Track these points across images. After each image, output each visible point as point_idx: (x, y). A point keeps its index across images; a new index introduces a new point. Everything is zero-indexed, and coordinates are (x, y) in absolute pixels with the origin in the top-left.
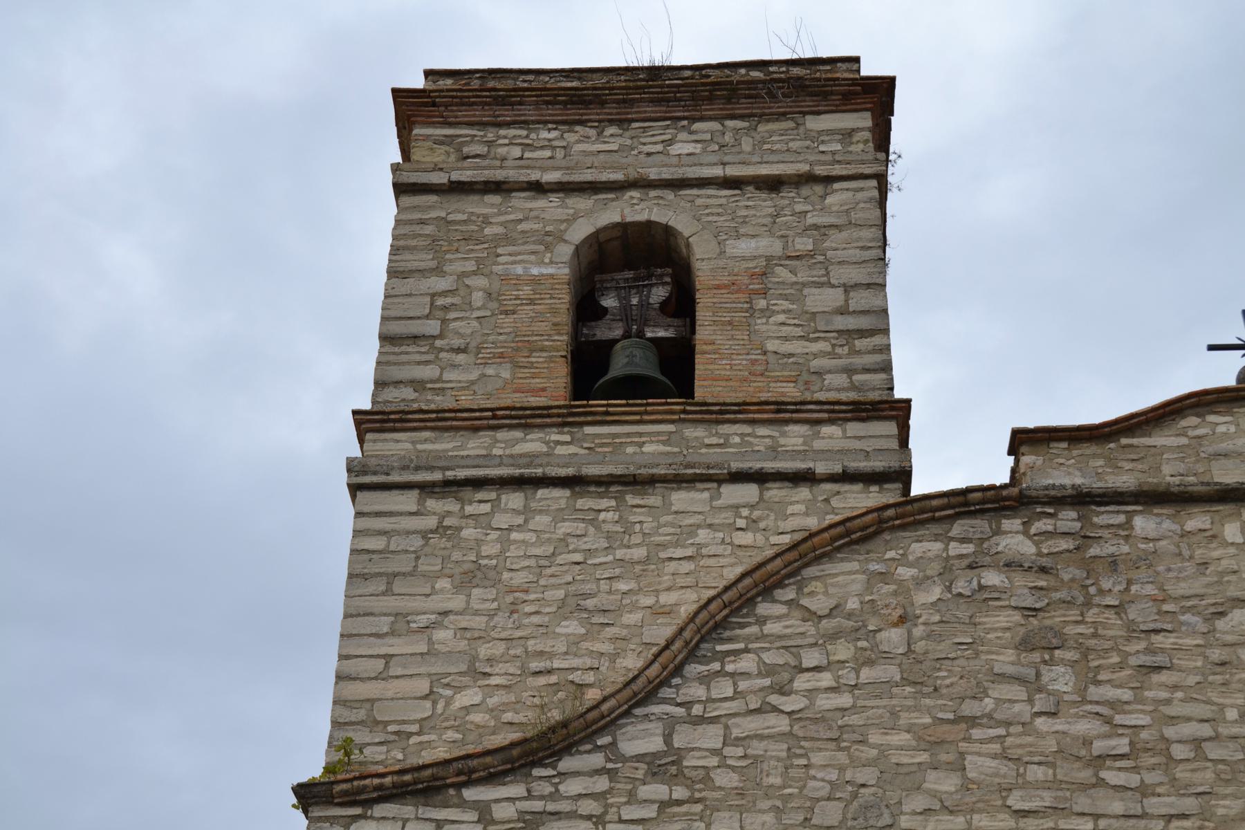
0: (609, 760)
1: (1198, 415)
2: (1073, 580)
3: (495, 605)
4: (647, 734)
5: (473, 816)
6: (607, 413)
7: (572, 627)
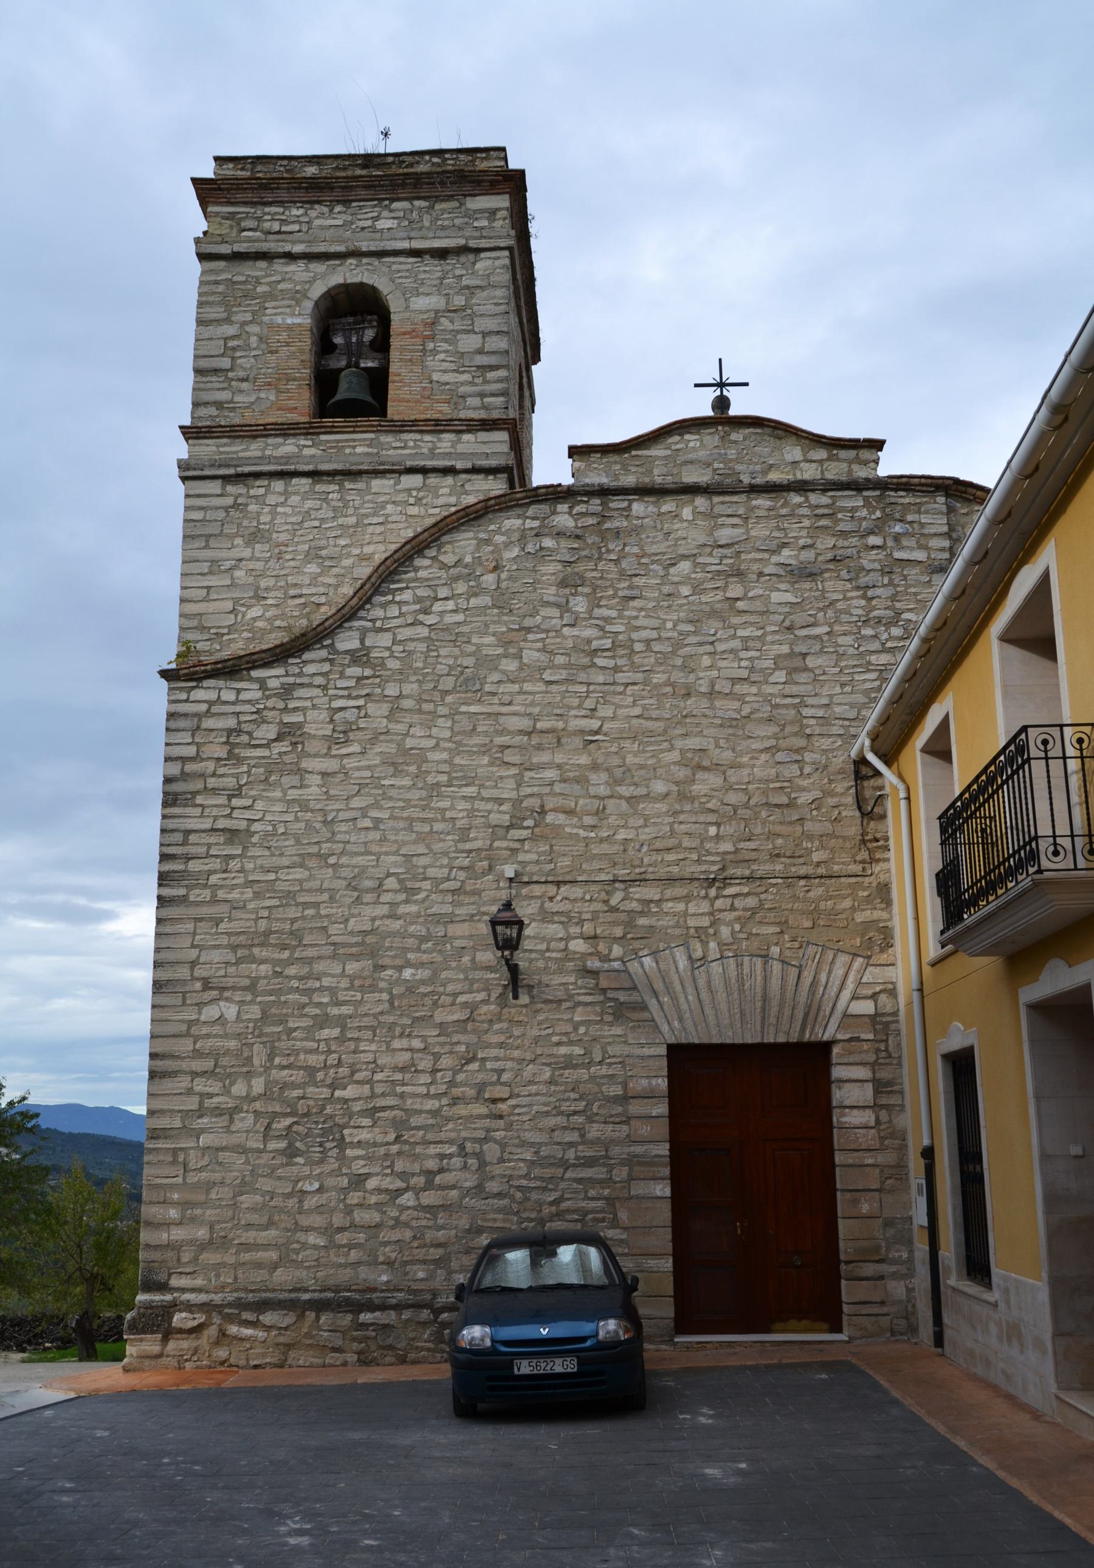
0: (330, 654)
1: (680, 435)
2: (593, 543)
3: (269, 555)
4: (351, 638)
5: (256, 686)
6: (334, 427)
7: (312, 568)
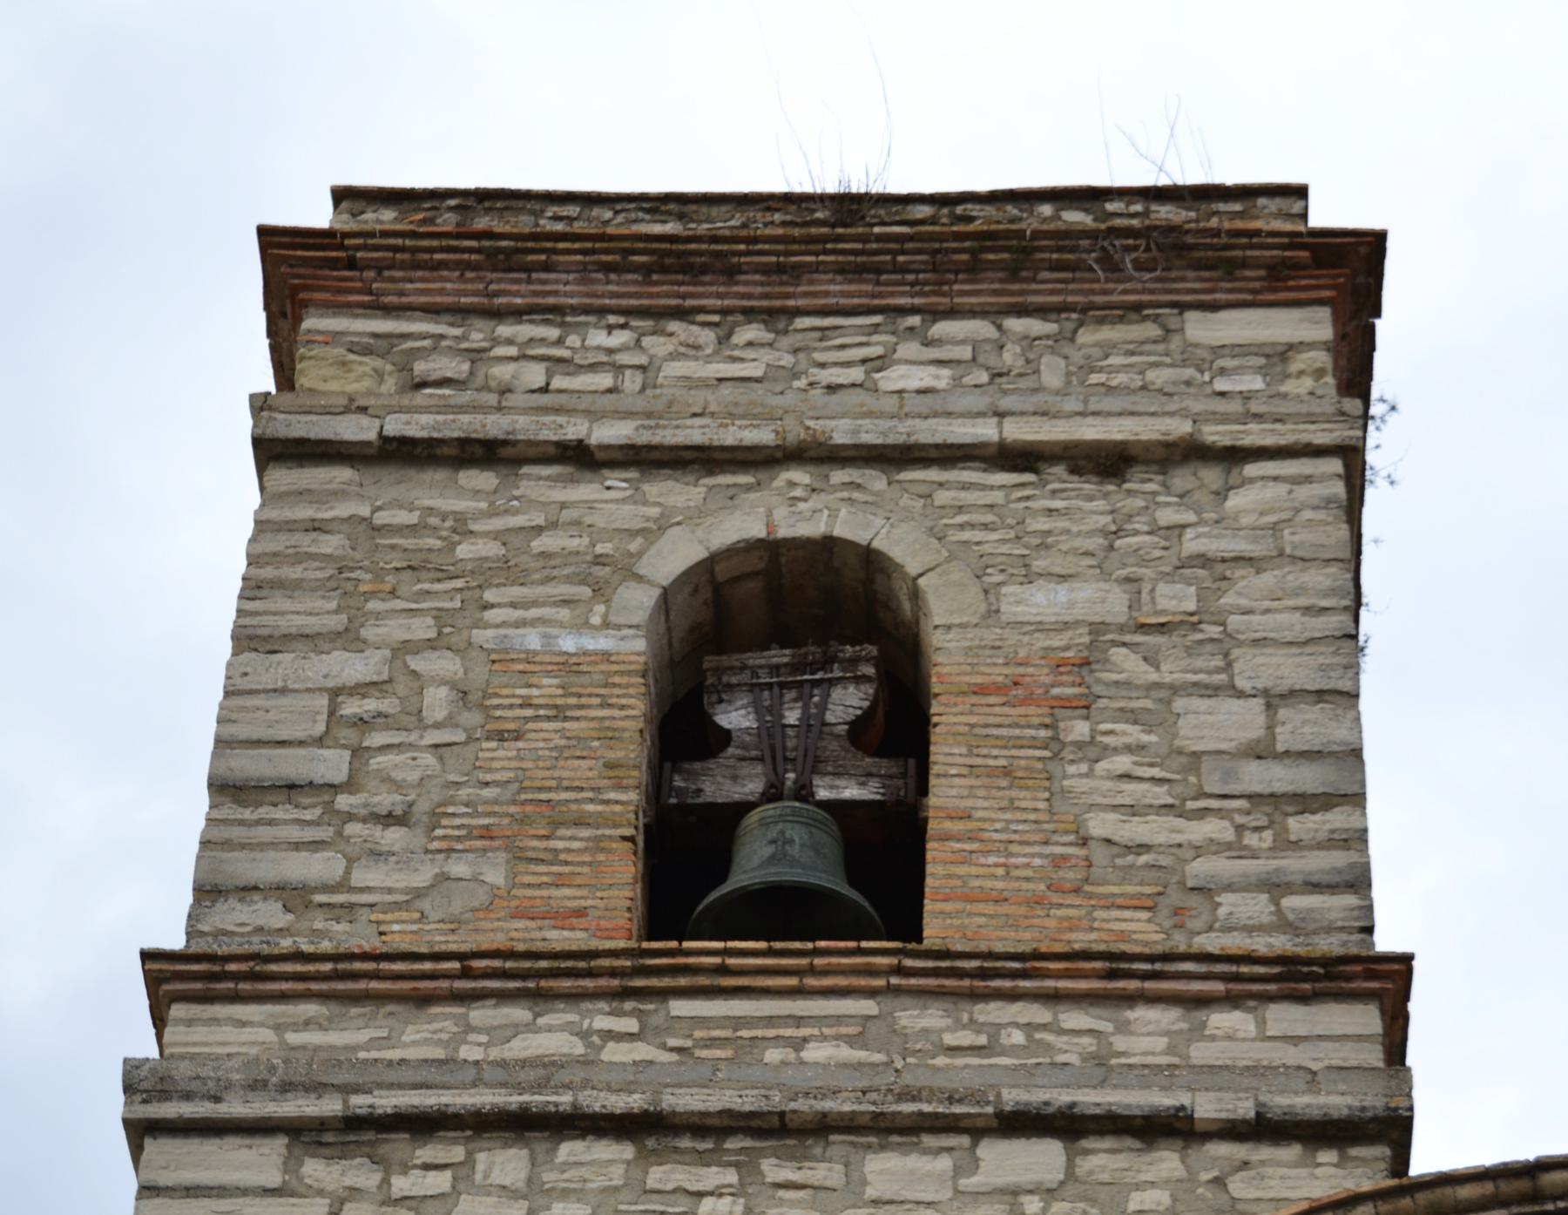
6: (723, 970)
